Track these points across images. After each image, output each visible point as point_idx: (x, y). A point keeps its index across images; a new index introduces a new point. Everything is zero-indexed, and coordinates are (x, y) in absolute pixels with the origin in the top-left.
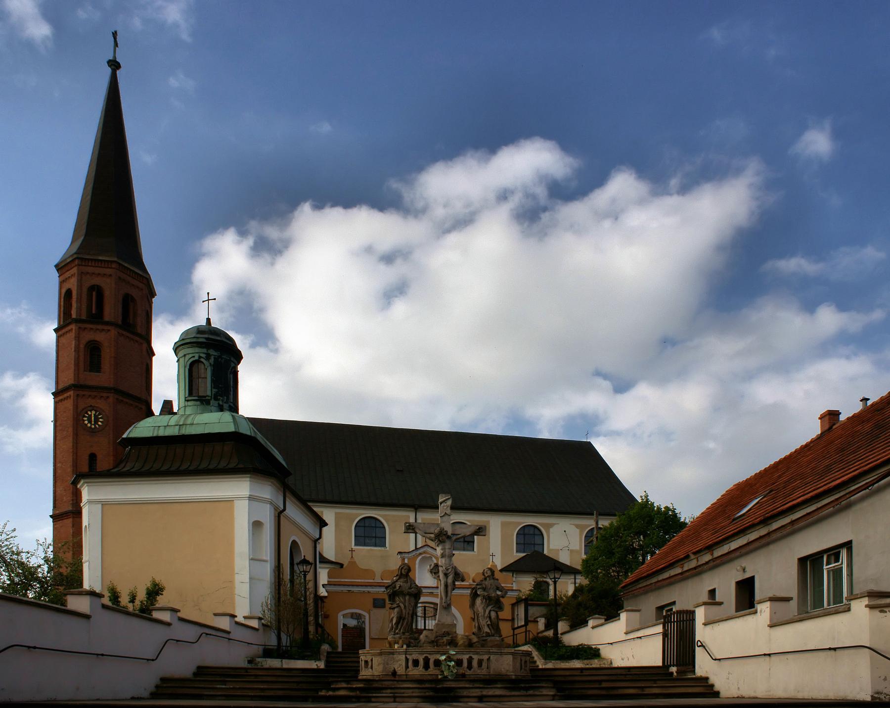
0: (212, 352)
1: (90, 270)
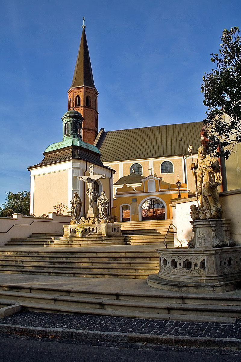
0: (71, 119)
1: (76, 91)
